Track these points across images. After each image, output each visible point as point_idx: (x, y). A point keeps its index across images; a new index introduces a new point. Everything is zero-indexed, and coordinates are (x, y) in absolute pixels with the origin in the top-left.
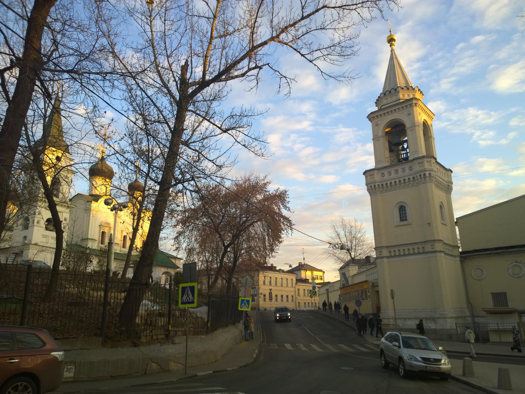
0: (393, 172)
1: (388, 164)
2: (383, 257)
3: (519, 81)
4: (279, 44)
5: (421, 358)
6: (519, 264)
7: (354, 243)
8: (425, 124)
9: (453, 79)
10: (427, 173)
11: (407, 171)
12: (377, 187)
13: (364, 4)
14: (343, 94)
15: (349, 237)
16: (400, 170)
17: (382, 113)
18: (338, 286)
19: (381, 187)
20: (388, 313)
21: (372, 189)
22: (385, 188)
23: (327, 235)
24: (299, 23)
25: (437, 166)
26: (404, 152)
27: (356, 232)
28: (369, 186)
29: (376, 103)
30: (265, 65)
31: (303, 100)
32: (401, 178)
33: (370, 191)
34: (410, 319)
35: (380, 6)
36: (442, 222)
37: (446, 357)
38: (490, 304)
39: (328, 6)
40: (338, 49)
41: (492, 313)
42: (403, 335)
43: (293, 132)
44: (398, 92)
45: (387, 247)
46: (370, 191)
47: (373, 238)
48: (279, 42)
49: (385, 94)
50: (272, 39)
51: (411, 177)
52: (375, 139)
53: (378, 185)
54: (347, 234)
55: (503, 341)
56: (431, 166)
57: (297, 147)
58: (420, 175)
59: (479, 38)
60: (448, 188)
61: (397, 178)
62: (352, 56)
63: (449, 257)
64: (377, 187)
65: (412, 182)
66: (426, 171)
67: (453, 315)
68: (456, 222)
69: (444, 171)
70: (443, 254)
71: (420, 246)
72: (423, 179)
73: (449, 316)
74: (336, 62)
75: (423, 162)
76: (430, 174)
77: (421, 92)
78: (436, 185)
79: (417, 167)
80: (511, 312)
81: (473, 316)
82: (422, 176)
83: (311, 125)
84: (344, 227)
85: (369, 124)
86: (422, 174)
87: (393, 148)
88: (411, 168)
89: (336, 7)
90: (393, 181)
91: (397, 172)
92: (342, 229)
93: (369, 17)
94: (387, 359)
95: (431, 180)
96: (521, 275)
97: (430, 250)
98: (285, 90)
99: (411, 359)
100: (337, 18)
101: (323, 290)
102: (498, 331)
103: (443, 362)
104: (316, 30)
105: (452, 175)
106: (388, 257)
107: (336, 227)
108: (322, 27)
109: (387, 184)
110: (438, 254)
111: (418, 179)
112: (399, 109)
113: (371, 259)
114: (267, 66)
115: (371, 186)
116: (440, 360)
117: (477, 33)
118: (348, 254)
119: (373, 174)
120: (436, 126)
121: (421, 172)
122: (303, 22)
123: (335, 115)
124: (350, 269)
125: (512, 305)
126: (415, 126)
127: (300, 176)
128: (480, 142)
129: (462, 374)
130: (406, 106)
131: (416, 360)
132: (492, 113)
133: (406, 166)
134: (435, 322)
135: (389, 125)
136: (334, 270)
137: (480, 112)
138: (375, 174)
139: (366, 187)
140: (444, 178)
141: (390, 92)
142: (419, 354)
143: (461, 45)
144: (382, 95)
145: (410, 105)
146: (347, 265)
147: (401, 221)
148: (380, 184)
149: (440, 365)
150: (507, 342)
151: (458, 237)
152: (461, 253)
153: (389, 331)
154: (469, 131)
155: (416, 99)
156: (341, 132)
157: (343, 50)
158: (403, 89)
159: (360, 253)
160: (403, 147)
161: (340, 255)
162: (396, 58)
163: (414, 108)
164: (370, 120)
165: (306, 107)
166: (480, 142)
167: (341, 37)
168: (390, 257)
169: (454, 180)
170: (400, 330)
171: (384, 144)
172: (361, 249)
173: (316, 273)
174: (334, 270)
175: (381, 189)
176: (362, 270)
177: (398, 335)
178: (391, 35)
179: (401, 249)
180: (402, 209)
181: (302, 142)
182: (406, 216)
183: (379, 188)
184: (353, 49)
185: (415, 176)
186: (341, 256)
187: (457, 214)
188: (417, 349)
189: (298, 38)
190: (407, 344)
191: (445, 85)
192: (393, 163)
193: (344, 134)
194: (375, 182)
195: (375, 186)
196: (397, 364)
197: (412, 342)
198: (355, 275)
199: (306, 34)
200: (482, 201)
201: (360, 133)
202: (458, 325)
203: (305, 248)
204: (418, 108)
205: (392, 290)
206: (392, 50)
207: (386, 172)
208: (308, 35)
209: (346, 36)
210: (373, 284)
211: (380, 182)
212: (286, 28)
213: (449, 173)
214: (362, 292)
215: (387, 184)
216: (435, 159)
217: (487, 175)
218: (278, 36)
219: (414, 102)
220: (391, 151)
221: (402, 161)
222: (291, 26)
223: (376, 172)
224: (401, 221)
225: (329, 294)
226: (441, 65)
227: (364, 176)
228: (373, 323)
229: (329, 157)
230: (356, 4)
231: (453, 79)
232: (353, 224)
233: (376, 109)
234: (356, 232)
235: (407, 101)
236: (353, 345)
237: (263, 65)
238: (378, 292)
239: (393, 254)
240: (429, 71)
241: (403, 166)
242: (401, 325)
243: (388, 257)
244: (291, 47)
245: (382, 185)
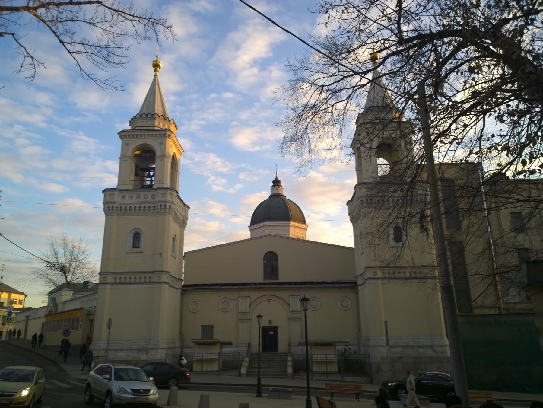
0: (135, 196)
1: (131, 187)
2: (106, 284)
3: (252, 142)
4: (35, 18)
5: (132, 390)
6: (229, 301)
7: (74, 265)
8: (174, 158)
9: (203, 123)
10: (168, 205)
11: (149, 199)
12: (115, 208)
13: (142, 19)
14: (91, 99)
15: (69, 258)
17: (135, 134)
18: (42, 313)
19: (119, 209)
20: (99, 345)
21: (109, 210)
22: (123, 212)
23: (45, 251)
24: (66, 6)
25: (178, 200)
26: (149, 179)
27: (79, 253)
28: (107, 205)
29: (130, 122)
30: (9, 34)
31: (40, 89)
32: (142, 204)
33: (107, 211)
34: (122, 350)
35: (157, 29)
36: (173, 255)
37: (155, 387)
38: (198, 336)
39: (103, 3)
40: (104, 52)
41: (199, 344)
42: (116, 367)
43: (18, 123)
44: (155, 119)
45: (113, 273)
46: (107, 211)
47: (100, 262)
48: (36, 16)
49: (141, 116)
50: (27, 8)
51: (152, 206)
52: (123, 158)
53: (117, 207)
54: (67, 254)
55: (204, 370)
56: (172, 198)
57: (21, 141)
58: (161, 205)
59: (228, 95)
60: (183, 223)
61: (137, 204)
62: (118, 66)
63: (171, 289)
64: (115, 208)
65: (152, 211)
66: (167, 202)
67: (165, 346)
68: (184, 256)
69: (181, 205)
70: (167, 286)
71: (148, 276)
72: (163, 210)
73: (161, 347)
74: (99, 65)
75: (166, 193)
76: (170, 206)
77: (176, 126)
78: (173, 218)
79: (159, 197)
80: (214, 343)
81: (182, 347)
82: (163, 207)
83: (44, 121)
84: (65, 246)
85: (119, 142)
86: (163, 204)
87: (139, 172)
88: (153, 197)
89: (112, 9)
90: (133, 206)
91: (138, 197)
92: (61, 248)
93: (143, 35)
94: (93, 394)
95: (170, 212)
96: (228, 310)
97: (157, 280)
98: (27, 72)
99: (120, 391)
100: (110, 20)
101: (22, 317)
102: (202, 361)
103: (151, 392)
104: (84, 21)
105: (189, 211)
106: (112, 284)
107: (55, 244)
108: (91, 22)
109: (126, 207)
110: (163, 285)
111: (158, 209)
112: (152, 135)
113: (90, 284)
114: (11, 36)
115: (109, 207)
116: (149, 391)
117: (228, 89)
118: (64, 277)
119: (113, 195)
120: (183, 162)
121: (163, 202)
122: (70, 7)
123: (76, 119)
124: (63, 294)
125: (217, 336)
126: (165, 156)
127: (17, 178)
128: (213, 186)
129: (386, 344)
130: (160, 135)
131: (126, 392)
132: (227, 163)
133: (149, 194)
134: (147, 354)
135: (139, 148)
136: (42, 294)
137: (218, 160)
138: (116, 195)
139: (103, 206)
140: (181, 212)
141: (147, 116)
142: (129, 386)
143: (213, 95)
144: (138, 116)
145: (164, 135)
146: (60, 288)
147: (133, 247)
148: (119, 206)
149: (149, 395)
150: (212, 371)
151: (183, 271)
152: (183, 286)
153: (100, 363)
154: (206, 174)
155: (170, 130)
156: (81, 140)
157: (105, 53)
158: (159, 117)
159: (77, 278)
160: (149, 174)
161: (53, 277)
162: (158, 85)
163: (167, 139)
164: (121, 137)
165: (43, 98)
166: (213, 186)
167: (110, 41)
168: (115, 284)
169: (189, 217)
170: (114, 362)
171: (131, 165)
172: (81, 273)
173: (14, 296)
174: (42, 294)
175: (118, 212)
176: (77, 296)
177: (110, 367)
178: (157, 61)
179: (128, 277)
180: (137, 236)
181: (28, 138)
182: (139, 244)
183: (117, 210)
184: (121, 58)
185: (156, 205)
186: (55, 278)
187: (187, 249)
188: (128, 380)
189: (60, 22)
190: (119, 377)
191: (194, 126)
192: (137, 187)
193: (84, 143)
194: (114, 203)
195: (113, 207)
196: (104, 398)
197: (123, 374)
198: (68, 301)
199: (70, 20)
200: (205, 240)
201: (103, 147)
202: (168, 356)
203: (7, 264)
204: (170, 140)
205: (110, 319)
206: (155, 76)
207: (127, 195)
208: (72, 22)
209: (116, 43)
210: (88, 311)
211: (120, 204)
212: (49, 4)
213: (187, 209)
214: (74, 321)
215: (126, 207)
216: (177, 193)
217: (213, 218)
218: (35, 9)
219: (168, 133)
220: (136, 174)
221: (145, 188)
222: (54, 4)
223: (117, 192)
224: (133, 247)
225: (29, 322)
226: (194, 106)
227: (103, 194)
228: (84, 354)
229: (60, 164)
230: (133, 16)
231: (203, 123)
232: (76, 244)
233: (129, 128)
234: (79, 253)
235: (161, 130)
236: (52, 381)
237: (6, 33)
238: (92, 321)
239: (118, 281)
240: (183, 108)
241: (146, 193)
242: (111, 357)
243: (112, 284)
244: (50, 27)
245: (121, 207)
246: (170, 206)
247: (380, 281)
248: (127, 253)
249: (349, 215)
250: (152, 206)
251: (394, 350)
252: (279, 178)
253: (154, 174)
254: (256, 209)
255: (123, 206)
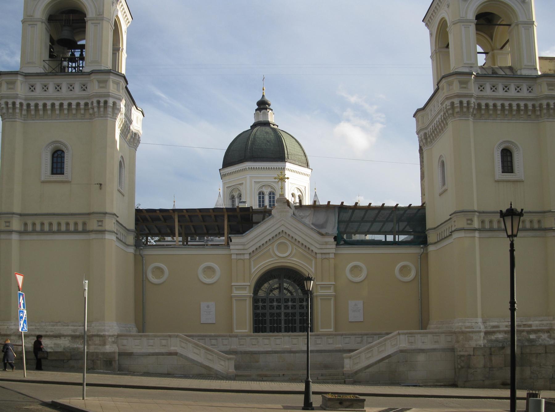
16: (51, 88)
26: (74, 65)
45: (21, 215)
56: (118, 90)
61: (57, 99)
76: (114, 103)
82: (102, 104)
86: (102, 100)
88: (84, 87)
106: (20, 233)
133: (77, 82)
147: (53, 173)
160: (73, 54)
207: (38, 83)
224: (53, 173)
246: (114, 103)
247: (477, 234)
248: (43, 182)
249: (418, 133)
250: (82, 103)
251: (493, 337)
252: (267, 98)
253: (81, 54)
254: (244, 132)
255: (32, 103)
